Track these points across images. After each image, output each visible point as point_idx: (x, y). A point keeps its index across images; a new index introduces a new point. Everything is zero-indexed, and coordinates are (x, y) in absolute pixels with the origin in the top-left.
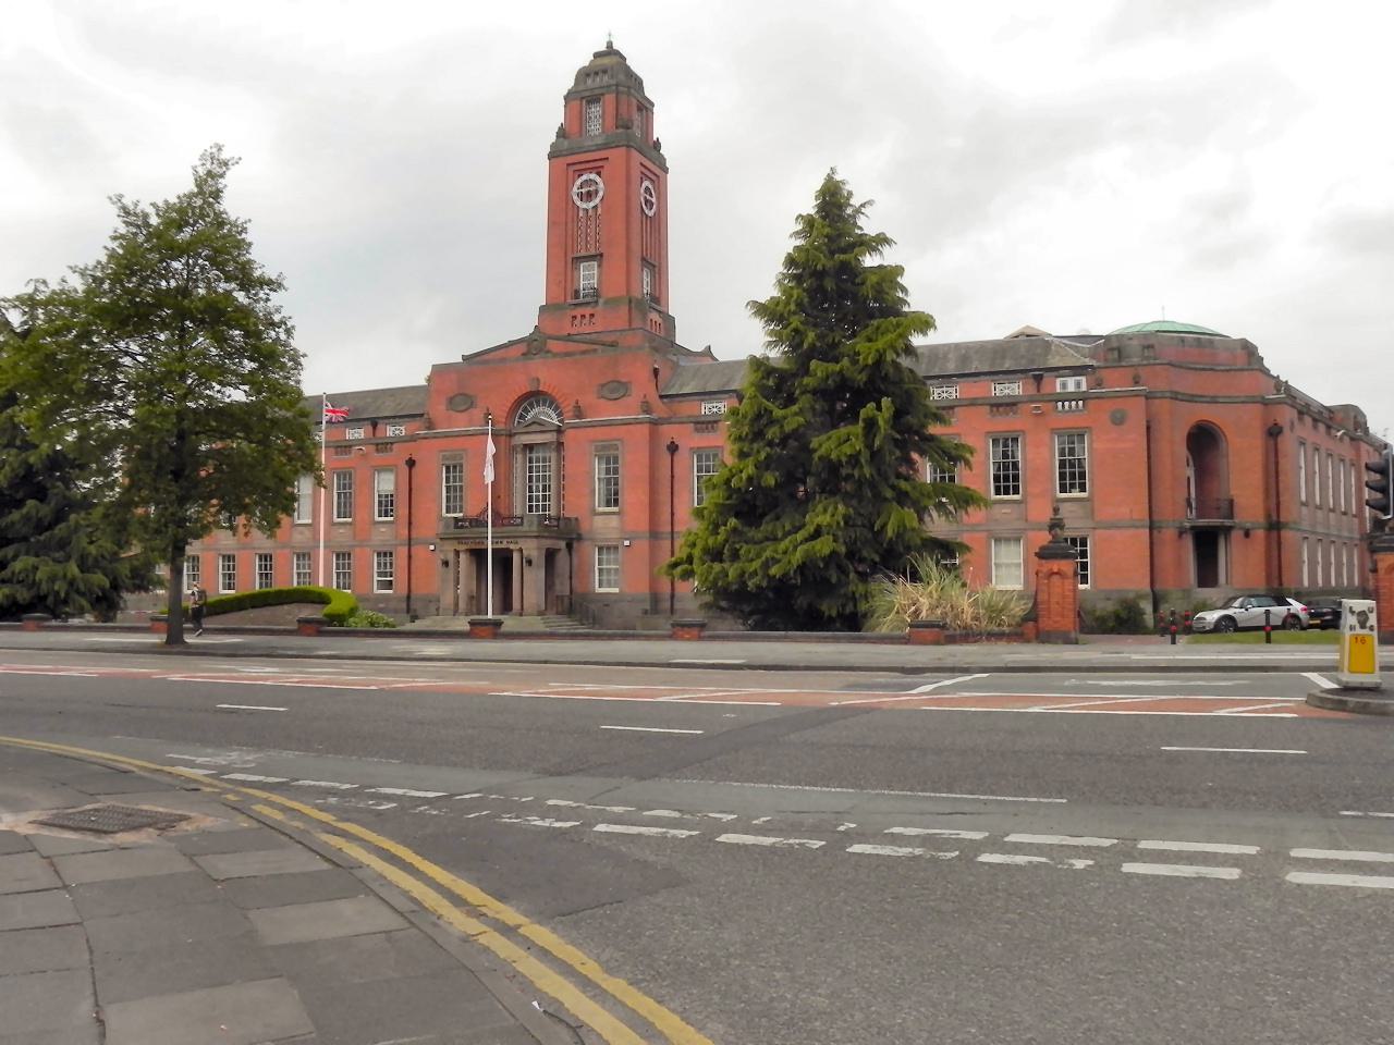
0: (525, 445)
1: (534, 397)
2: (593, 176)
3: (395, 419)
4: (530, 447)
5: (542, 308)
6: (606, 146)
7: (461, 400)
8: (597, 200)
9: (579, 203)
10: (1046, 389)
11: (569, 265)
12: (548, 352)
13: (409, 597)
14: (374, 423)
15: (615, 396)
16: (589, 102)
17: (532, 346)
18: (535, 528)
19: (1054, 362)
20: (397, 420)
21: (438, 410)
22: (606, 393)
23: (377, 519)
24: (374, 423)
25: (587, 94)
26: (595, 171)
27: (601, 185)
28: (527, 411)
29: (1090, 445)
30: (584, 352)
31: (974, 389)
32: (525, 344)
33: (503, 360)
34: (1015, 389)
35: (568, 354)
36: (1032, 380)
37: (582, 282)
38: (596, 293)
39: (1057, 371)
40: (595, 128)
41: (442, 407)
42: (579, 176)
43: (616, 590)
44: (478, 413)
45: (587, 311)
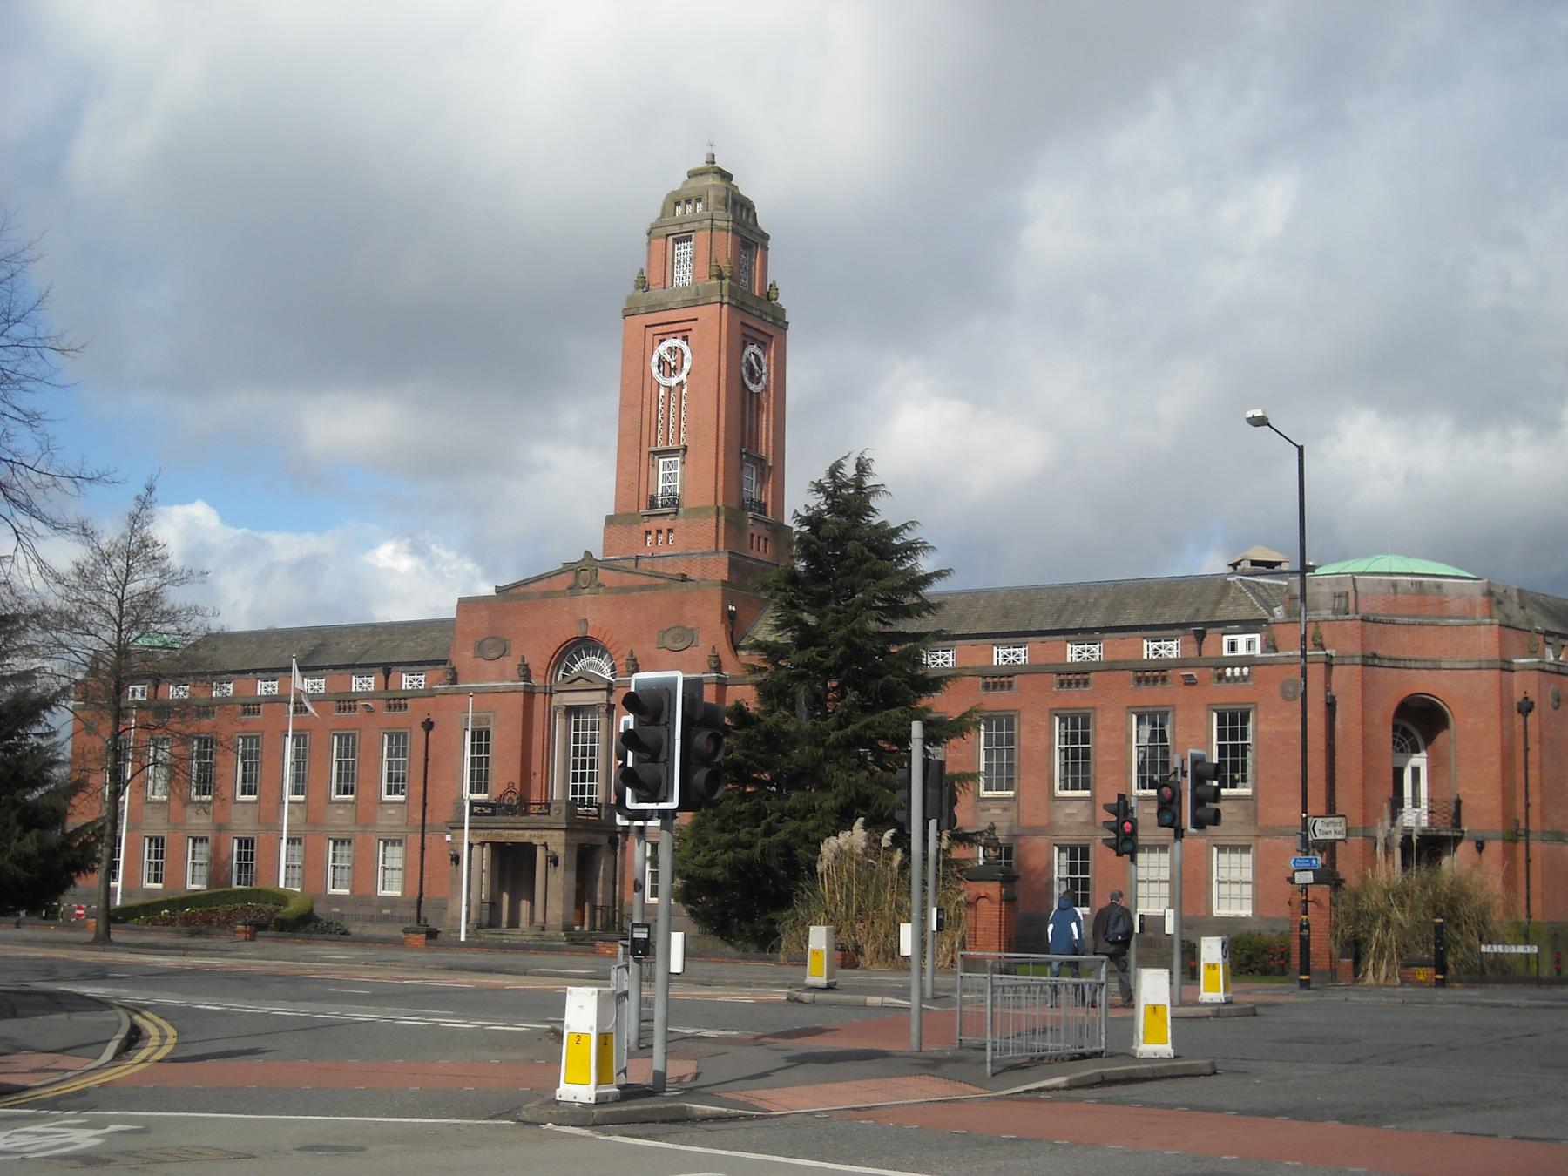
0: (568, 707)
1: (582, 644)
2: (678, 343)
3: (412, 665)
4: (573, 710)
5: (610, 520)
6: (694, 303)
7: (494, 646)
8: (683, 377)
9: (659, 378)
10: (1208, 651)
11: (644, 462)
12: (599, 586)
13: (420, 902)
14: (387, 669)
15: (679, 646)
16: (677, 241)
17: (582, 574)
18: (562, 818)
19: (1224, 613)
20: (416, 668)
21: (464, 657)
22: (668, 641)
23: (386, 797)
24: (387, 669)
25: (676, 229)
26: (680, 335)
27: (688, 355)
28: (574, 663)
29: (1256, 724)
30: (643, 588)
31: (1121, 647)
32: (572, 574)
33: (546, 595)
34: (1172, 649)
35: (625, 590)
36: (1192, 638)
37: (660, 485)
38: (674, 503)
39: (1224, 625)
40: (683, 276)
41: (469, 654)
42: (662, 341)
43: (347, 892)
44: (511, 663)
45: (665, 523)
